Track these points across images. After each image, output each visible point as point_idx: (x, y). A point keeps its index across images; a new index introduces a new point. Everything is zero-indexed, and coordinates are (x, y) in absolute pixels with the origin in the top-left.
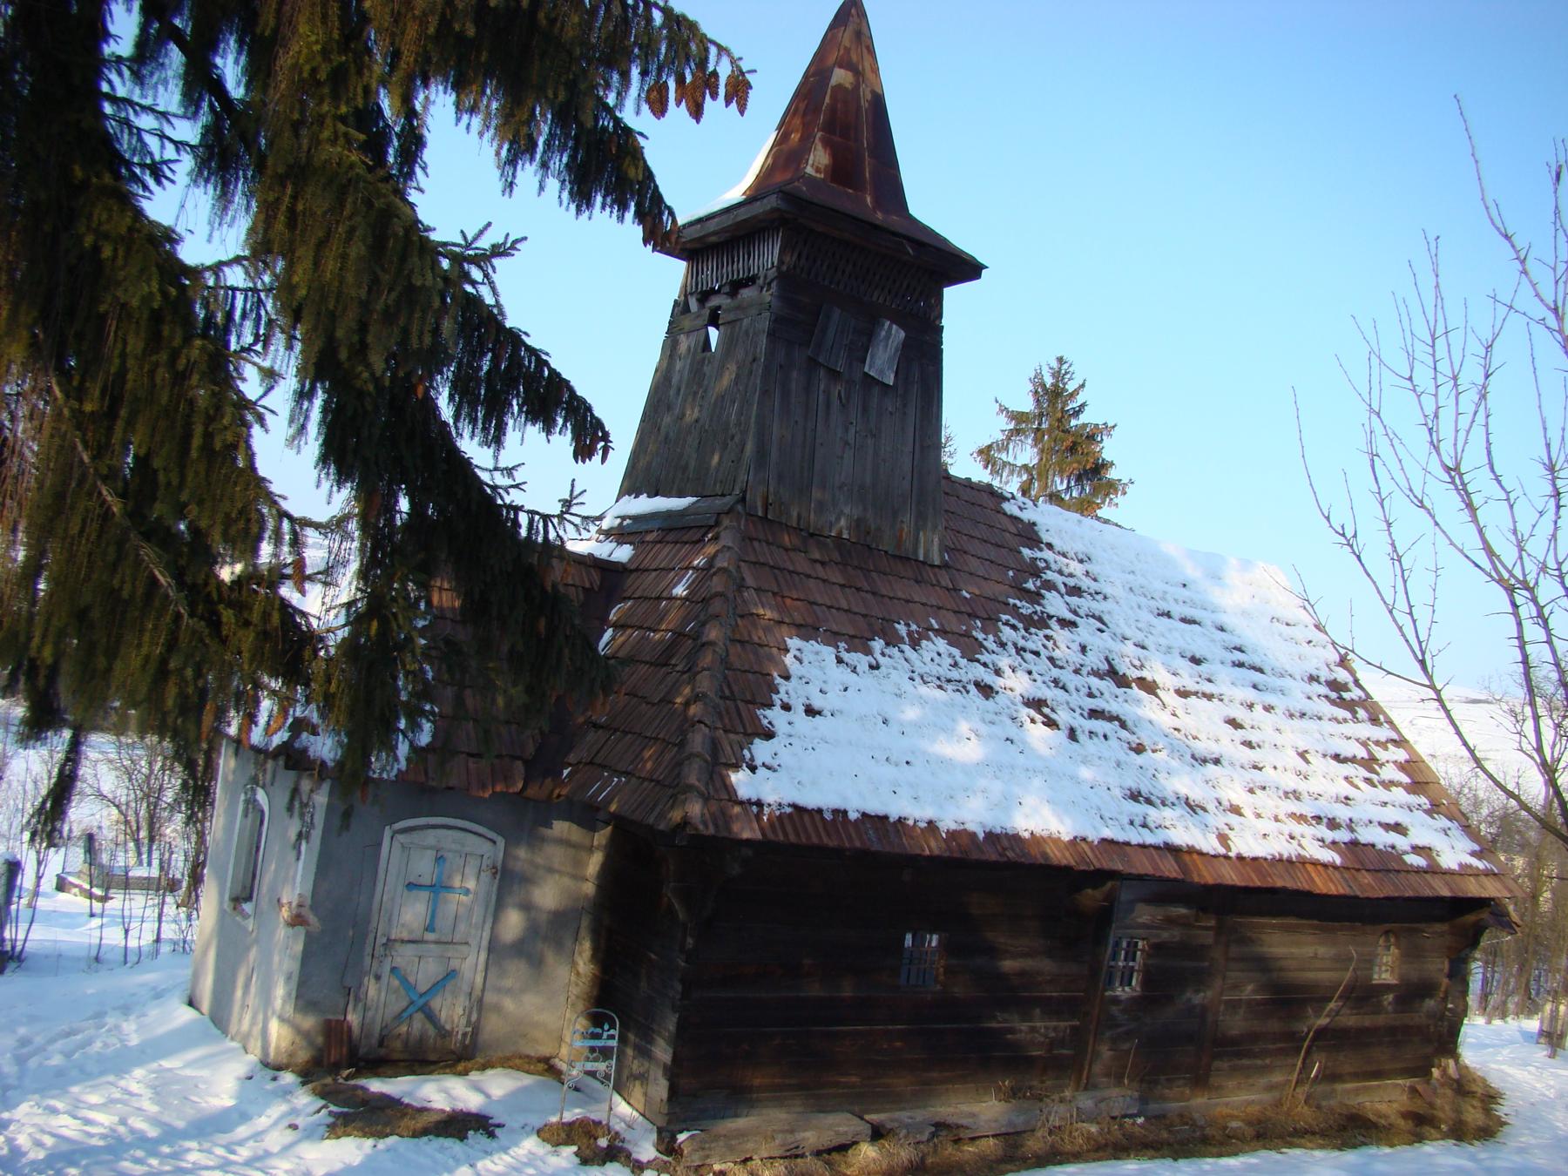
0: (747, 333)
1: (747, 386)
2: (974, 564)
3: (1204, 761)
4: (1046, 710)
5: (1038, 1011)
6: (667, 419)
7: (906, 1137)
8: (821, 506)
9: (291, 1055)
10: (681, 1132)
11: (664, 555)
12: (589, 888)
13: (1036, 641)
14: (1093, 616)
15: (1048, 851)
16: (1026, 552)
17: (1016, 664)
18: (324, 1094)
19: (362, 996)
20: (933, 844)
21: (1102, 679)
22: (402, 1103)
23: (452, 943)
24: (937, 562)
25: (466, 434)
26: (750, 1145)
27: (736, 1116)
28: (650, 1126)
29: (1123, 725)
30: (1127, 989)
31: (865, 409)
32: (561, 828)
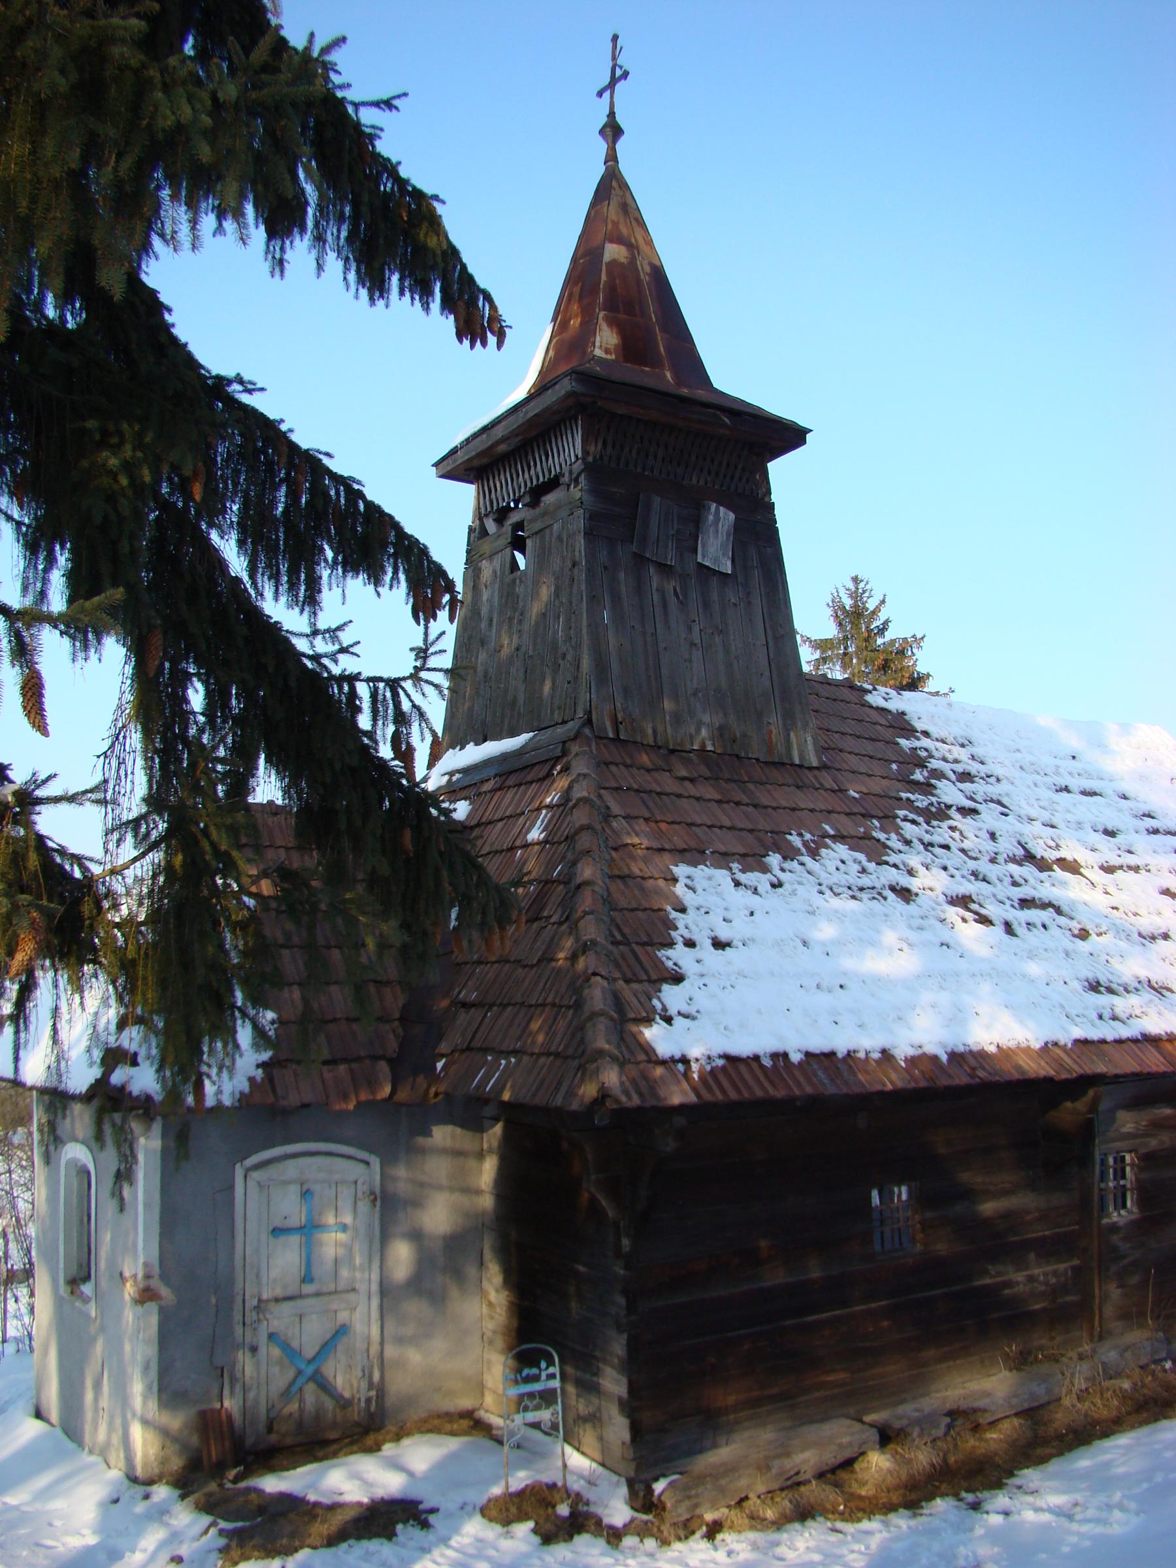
0: (560, 538)
1: (571, 594)
2: (853, 762)
3: (1153, 938)
4: (974, 906)
5: (1032, 1256)
6: (482, 656)
7: (921, 1435)
8: (677, 719)
9: (163, 1461)
10: (656, 1479)
11: (508, 801)
12: (487, 1202)
13: (941, 833)
14: (992, 801)
15: (1021, 1062)
16: (903, 742)
17: (929, 861)
18: (208, 1507)
19: (239, 1375)
20: (894, 1076)
21: (1021, 865)
22: (308, 1502)
23: (336, 1292)
24: (815, 764)
25: (269, 593)
26: (743, 1482)
27: (715, 1446)
28: (615, 1478)
29: (1059, 911)
30: (1123, 1212)
31: (706, 605)
32: (442, 1135)
